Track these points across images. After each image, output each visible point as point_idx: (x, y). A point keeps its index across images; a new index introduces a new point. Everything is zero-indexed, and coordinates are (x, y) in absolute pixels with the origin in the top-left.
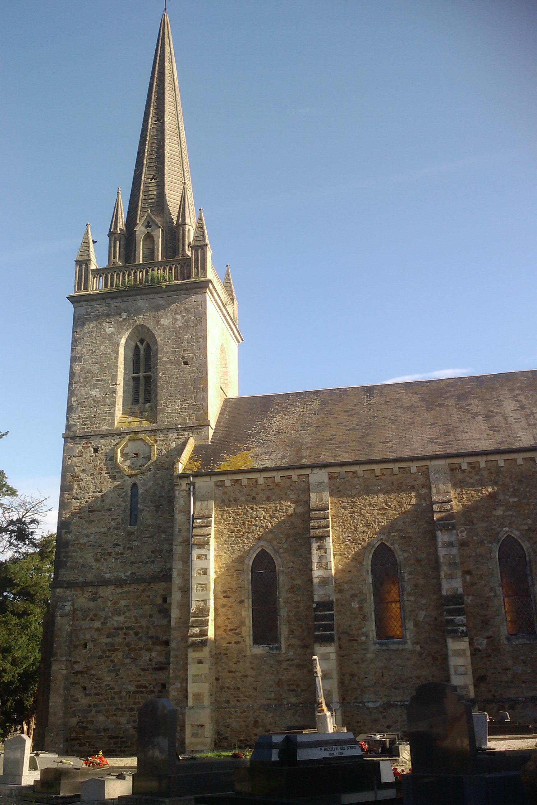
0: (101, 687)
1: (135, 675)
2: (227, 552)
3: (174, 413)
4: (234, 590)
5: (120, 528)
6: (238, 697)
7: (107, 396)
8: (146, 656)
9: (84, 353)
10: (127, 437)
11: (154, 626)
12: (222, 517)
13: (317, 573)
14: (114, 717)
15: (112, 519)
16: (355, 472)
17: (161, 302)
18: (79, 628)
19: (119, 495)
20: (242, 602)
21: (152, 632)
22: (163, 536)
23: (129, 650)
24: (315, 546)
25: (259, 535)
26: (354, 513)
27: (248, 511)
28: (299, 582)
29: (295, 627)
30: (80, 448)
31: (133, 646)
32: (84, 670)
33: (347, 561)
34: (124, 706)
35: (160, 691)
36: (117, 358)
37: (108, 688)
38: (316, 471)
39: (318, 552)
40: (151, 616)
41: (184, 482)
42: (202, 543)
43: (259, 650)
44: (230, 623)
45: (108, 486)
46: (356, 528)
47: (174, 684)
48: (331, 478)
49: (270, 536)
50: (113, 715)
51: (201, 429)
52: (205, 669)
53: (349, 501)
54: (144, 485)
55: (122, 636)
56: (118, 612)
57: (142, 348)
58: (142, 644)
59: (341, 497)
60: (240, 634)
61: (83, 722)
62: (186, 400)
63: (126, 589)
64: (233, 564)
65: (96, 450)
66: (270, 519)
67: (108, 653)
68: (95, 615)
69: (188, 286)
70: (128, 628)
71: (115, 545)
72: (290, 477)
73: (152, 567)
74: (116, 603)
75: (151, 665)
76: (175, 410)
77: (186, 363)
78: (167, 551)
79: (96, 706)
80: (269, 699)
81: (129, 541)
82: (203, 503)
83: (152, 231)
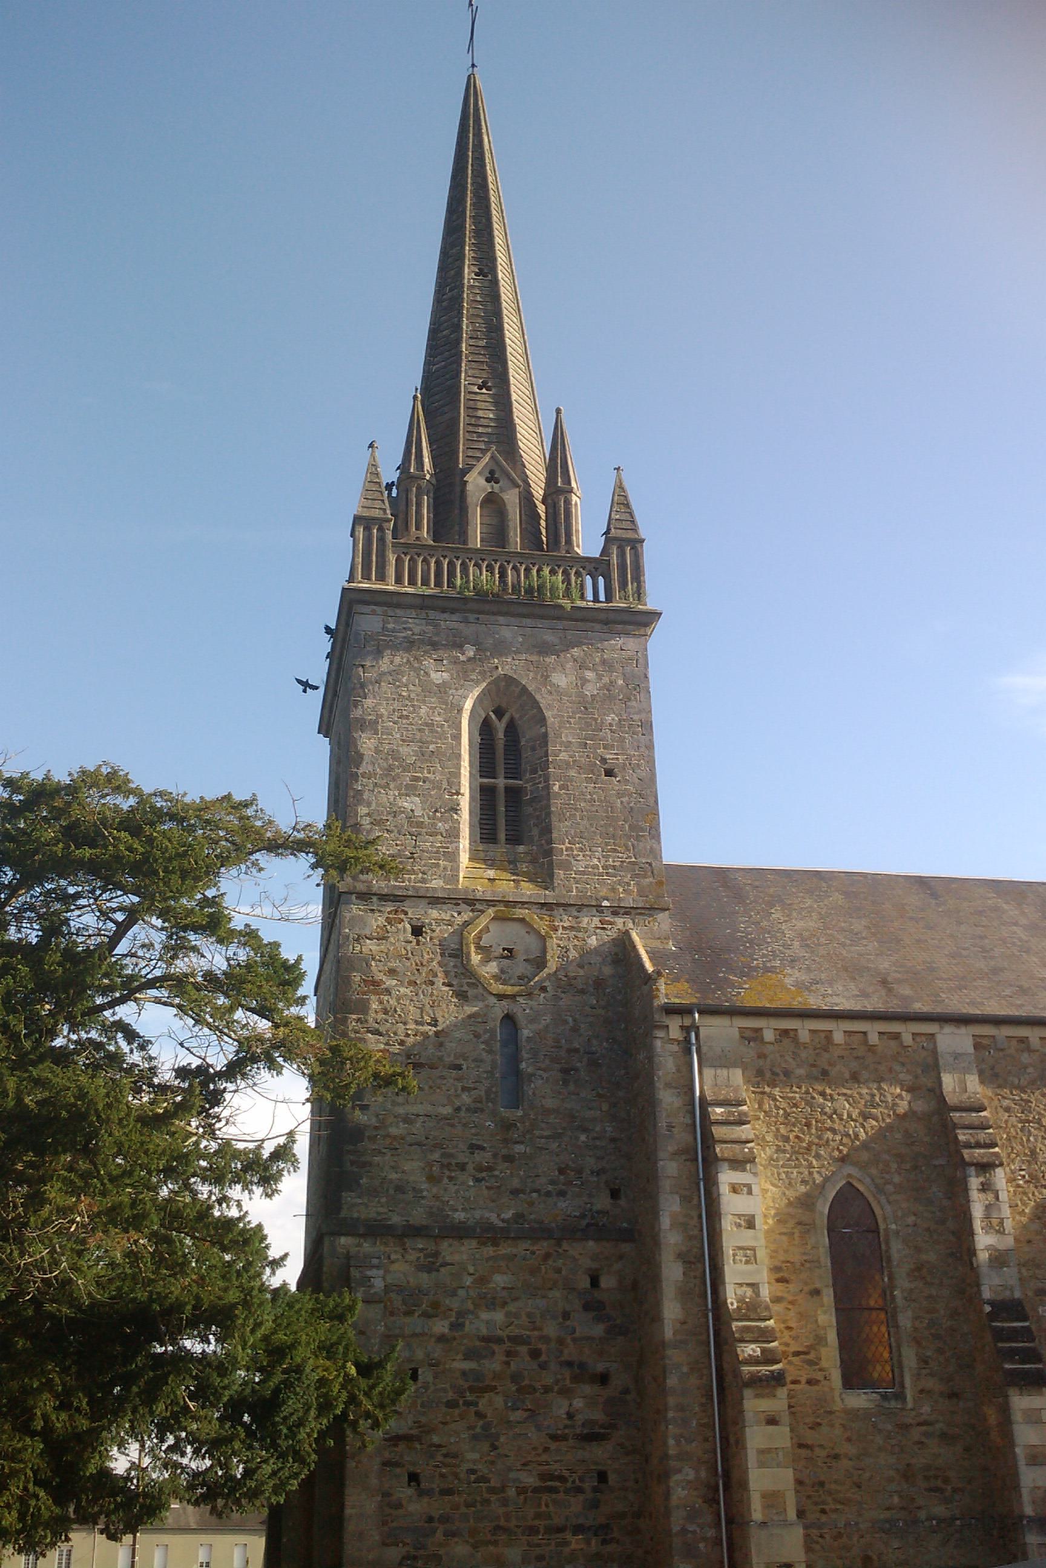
0: (456, 1475)
1: (535, 1449)
2: (776, 1182)
3: (589, 873)
4: (798, 1266)
5: (482, 1110)
6: (824, 1503)
7: (438, 814)
8: (560, 1407)
9: (381, 716)
10: (491, 912)
11: (574, 1340)
12: (760, 1107)
13: (984, 1240)
14: (491, 1548)
15: (464, 1089)
16: (1023, 1040)
17: (549, 637)
18: (397, 1331)
19: (477, 1036)
20: (816, 1292)
21: (570, 1352)
22: (583, 1138)
23: (518, 1390)
24: (974, 1182)
25: (840, 1151)
26: (1029, 1122)
27: (814, 1098)
28: (931, 1257)
29: (929, 1354)
30: (381, 921)
31: (526, 1382)
32: (414, 1432)
33: (1024, 1220)
34: (514, 1522)
35: (595, 1490)
36: (457, 737)
37: (473, 1477)
38: (948, 1029)
39: (982, 1196)
40: (566, 1315)
41: (675, 1026)
42: (740, 1157)
43: (860, 1400)
44: (795, 1338)
45: (450, 1013)
46: (1033, 1152)
47: (680, 1471)
48: (977, 1046)
49: (865, 1156)
50: (490, 1542)
51: (651, 916)
52: (782, 1437)
53: (1017, 1098)
54: (532, 1020)
55: (500, 1357)
56: (492, 1303)
57: (500, 726)
58: (549, 1380)
59: (999, 1087)
60: (817, 1364)
61: (415, 1558)
62: (615, 851)
63: (505, 1249)
64: (791, 1210)
65: (417, 931)
66: (861, 1120)
67: (469, 1397)
68: (435, 1305)
69: (612, 616)
70: (516, 1340)
71: (474, 1148)
72: (896, 1036)
73: (562, 1204)
74: (482, 1280)
75: (573, 1427)
76: (593, 867)
77: (609, 773)
78: (592, 1173)
79: (445, 1519)
80: (888, 1509)
81: (506, 1141)
82: (719, 1071)
83: (502, 490)
